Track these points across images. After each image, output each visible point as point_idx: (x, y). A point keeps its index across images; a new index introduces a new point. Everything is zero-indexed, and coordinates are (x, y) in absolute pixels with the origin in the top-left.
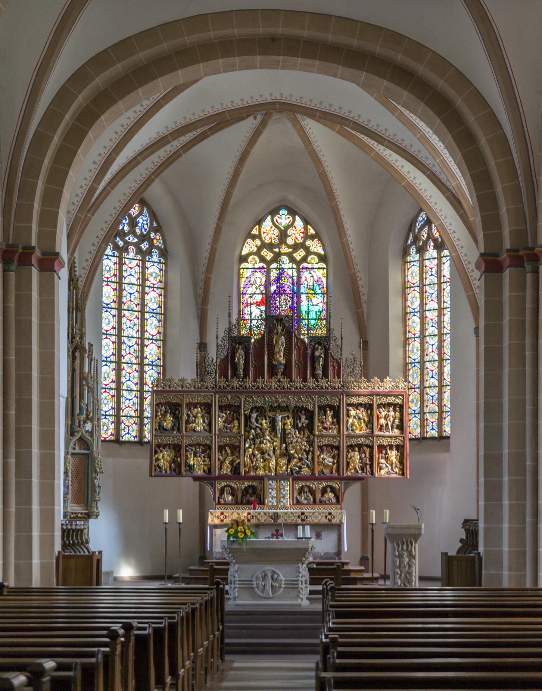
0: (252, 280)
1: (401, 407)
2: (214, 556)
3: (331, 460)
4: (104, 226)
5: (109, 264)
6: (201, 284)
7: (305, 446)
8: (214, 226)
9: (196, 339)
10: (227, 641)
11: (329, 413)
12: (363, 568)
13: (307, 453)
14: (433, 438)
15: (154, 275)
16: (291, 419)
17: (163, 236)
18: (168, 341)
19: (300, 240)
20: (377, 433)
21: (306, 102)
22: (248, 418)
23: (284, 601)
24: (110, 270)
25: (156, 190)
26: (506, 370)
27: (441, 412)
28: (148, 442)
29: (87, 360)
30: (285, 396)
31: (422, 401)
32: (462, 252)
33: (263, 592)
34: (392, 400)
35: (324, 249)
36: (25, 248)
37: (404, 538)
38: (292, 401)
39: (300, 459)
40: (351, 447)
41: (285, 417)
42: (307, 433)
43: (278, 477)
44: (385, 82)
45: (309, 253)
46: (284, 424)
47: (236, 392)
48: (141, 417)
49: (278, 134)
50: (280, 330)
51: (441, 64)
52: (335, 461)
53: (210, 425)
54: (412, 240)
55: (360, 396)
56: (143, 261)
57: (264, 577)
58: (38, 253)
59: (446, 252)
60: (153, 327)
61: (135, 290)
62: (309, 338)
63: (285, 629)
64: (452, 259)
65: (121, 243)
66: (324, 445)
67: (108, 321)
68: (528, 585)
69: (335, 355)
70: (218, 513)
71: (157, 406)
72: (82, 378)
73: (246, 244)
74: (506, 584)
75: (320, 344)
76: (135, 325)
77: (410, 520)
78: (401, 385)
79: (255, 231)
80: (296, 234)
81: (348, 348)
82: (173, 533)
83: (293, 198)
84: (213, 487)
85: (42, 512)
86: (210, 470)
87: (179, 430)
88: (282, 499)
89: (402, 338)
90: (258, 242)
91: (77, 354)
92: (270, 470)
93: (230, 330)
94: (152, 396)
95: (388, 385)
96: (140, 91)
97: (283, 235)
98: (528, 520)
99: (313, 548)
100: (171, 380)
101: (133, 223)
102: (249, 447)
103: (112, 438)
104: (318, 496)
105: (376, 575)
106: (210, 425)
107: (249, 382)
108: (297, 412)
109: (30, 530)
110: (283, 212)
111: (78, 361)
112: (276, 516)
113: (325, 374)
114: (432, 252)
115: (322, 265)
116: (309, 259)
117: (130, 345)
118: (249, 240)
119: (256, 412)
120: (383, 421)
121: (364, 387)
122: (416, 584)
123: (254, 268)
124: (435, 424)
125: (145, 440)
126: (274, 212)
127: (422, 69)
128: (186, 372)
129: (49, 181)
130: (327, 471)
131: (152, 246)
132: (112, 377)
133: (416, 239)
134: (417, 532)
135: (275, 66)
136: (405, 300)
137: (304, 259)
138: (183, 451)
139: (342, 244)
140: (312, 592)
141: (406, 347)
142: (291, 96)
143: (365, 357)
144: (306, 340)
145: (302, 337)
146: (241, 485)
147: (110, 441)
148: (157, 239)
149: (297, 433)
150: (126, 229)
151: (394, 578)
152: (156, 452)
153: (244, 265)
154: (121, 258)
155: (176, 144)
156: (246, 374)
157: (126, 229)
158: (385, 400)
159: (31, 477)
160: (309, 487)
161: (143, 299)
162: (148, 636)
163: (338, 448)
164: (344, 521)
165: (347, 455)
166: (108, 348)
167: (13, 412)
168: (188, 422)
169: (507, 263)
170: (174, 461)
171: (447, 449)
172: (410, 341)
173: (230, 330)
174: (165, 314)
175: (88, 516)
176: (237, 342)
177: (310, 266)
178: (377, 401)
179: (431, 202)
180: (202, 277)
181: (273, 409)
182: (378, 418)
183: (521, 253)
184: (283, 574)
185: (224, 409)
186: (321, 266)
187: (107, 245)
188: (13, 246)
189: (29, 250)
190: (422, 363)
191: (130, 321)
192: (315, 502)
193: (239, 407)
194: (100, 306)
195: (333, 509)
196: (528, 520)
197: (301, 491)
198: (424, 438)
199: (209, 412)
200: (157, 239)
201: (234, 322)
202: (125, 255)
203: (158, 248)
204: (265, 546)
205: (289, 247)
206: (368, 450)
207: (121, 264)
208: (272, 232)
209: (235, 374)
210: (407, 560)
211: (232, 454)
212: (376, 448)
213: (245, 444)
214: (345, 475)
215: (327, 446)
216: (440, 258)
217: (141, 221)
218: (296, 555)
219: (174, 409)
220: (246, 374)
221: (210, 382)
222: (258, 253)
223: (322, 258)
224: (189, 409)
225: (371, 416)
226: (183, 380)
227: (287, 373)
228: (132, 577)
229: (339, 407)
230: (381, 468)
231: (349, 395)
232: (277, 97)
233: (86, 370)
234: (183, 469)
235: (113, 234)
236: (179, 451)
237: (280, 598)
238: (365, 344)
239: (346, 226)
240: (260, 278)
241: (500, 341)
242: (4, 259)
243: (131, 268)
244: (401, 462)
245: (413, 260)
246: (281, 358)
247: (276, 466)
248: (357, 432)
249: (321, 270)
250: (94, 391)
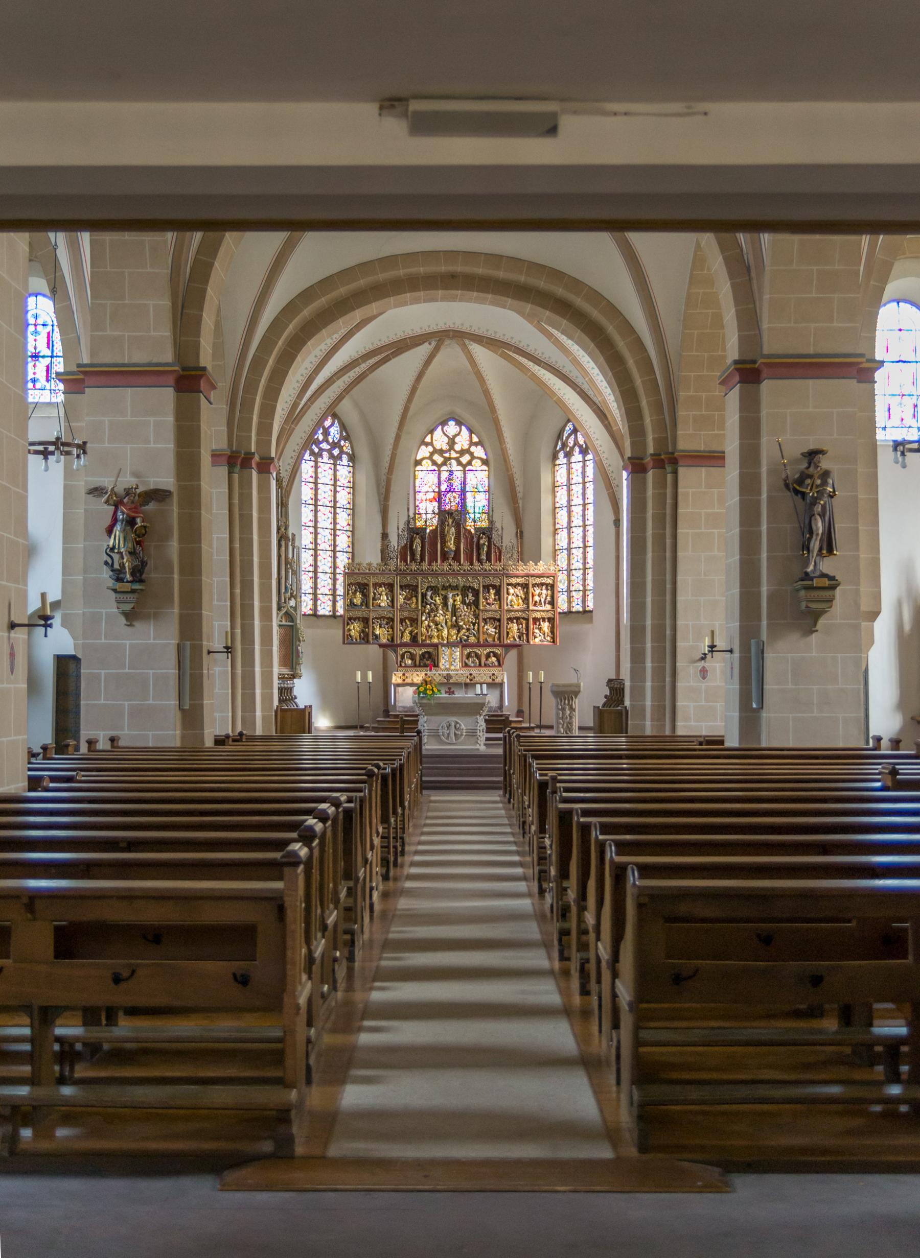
0: (426, 481)
1: (552, 586)
4: (303, 435)
5: (307, 468)
6: (384, 484)
7: (471, 618)
8: (394, 435)
9: (379, 530)
10: (424, 779)
12: (521, 719)
13: (474, 625)
14: (578, 612)
17: (351, 443)
18: (356, 532)
19: (466, 447)
20: (531, 607)
21: (475, 330)
22: (424, 596)
23: (464, 746)
25: (346, 407)
26: (649, 555)
27: (585, 591)
28: (341, 616)
29: (290, 548)
31: (569, 581)
32: (604, 456)
33: (447, 738)
34: (545, 580)
36: (246, 454)
37: (566, 695)
38: (461, 581)
39: (468, 630)
40: (510, 620)
42: (473, 608)
43: (450, 645)
44: (548, 313)
45: (473, 457)
46: (454, 601)
47: (414, 574)
48: (334, 595)
49: (450, 357)
51: (595, 297)
53: (392, 601)
54: (560, 446)
55: (517, 577)
56: (335, 465)
57: (449, 727)
58: (257, 458)
59: (590, 457)
60: (343, 519)
62: (475, 529)
63: (468, 769)
64: (595, 462)
65: (316, 450)
67: (307, 514)
68: (668, 733)
70: (400, 674)
71: (348, 586)
72: (287, 562)
74: (648, 732)
75: (484, 534)
77: (571, 679)
78: (552, 568)
79: (428, 439)
80: (463, 441)
81: (507, 537)
82: (364, 690)
83: (459, 411)
84: (396, 652)
85: (263, 673)
86: (393, 638)
87: (367, 606)
89: (552, 529)
90: (430, 449)
91: (283, 543)
92: (443, 639)
94: (344, 577)
95: (541, 568)
96: (341, 320)
97: (452, 442)
98: (668, 679)
99: (489, 702)
100: (359, 564)
101: (326, 433)
103: (311, 612)
104: (483, 659)
105: (532, 725)
106: (392, 601)
107: (425, 566)
108: (465, 590)
109: (254, 688)
110: (452, 423)
111: (283, 548)
113: (489, 559)
114: (577, 456)
115: (485, 468)
116: (474, 462)
117: (325, 536)
118: (423, 447)
120: (537, 598)
121: (522, 569)
122: (576, 733)
124: (580, 600)
125: (338, 614)
126: (444, 423)
127: (579, 302)
128: (371, 557)
129: (265, 396)
130: (490, 640)
131: (342, 452)
133: (564, 445)
134: (577, 689)
135: (453, 299)
136: (555, 497)
137: (469, 463)
138: (371, 623)
139: (502, 450)
140: (487, 739)
142: (462, 324)
143: (522, 543)
144: (473, 531)
145: (468, 528)
147: (309, 615)
148: (346, 445)
150: (321, 438)
151: (558, 727)
152: (348, 624)
153: (418, 468)
154: (316, 462)
155: (364, 366)
156: (422, 559)
157: (321, 438)
158: (538, 581)
159: (254, 644)
160: (494, 653)
162: (388, 773)
163: (499, 620)
164: (505, 680)
166: (306, 538)
167: (238, 591)
168: (374, 599)
169: (651, 465)
170: (363, 631)
171: (590, 620)
172: (559, 531)
173: (409, 522)
174: (353, 509)
175: (293, 676)
176: (414, 532)
178: (532, 581)
179: (578, 414)
180: (384, 478)
181: (444, 588)
182: (533, 596)
183: (663, 457)
184: (464, 724)
187: (306, 451)
188: (238, 452)
189: (249, 457)
190: (569, 549)
192: (480, 665)
193: (417, 586)
194: (300, 503)
195: (496, 671)
196: (668, 679)
197: (469, 656)
198: (570, 612)
199: (392, 591)
200: (346, 445)
201: (411, 515)
202: (320, 459)
203: (347, 454)
204: (461, 701)
205: (457, 452)
206: (524, 622)
207: (316, 467)
209: (413, 559)
210: (568, 712)
211: (411, 626)
212: (531, 621)
215: (490, 618)
216: (584, 461)
218: (474, 708)
219: (363, 588)
220: (422, 559)
221: (392, 565)
222: (430, 458)
223: (485, 462)
224: (375, 588)
225: (527, 594)
226: (370, 564)
227: (457, 558)
228: (329, 727)
229: (500, 586)
230: (535, 637)
231: (509, 576)
232: (450, 325)
233: (290, 556)
234: (371, 637)
235: (310, 441)
236: (367, 623)
237: (461, 744)
238: (520, 534)
239: (505, 435)
240: (433, 478)
241: (644, 530)
242: (229, 463)
244: (552, 632)
246: (451, 545)
248: (515, 607)
250: (296, 573)
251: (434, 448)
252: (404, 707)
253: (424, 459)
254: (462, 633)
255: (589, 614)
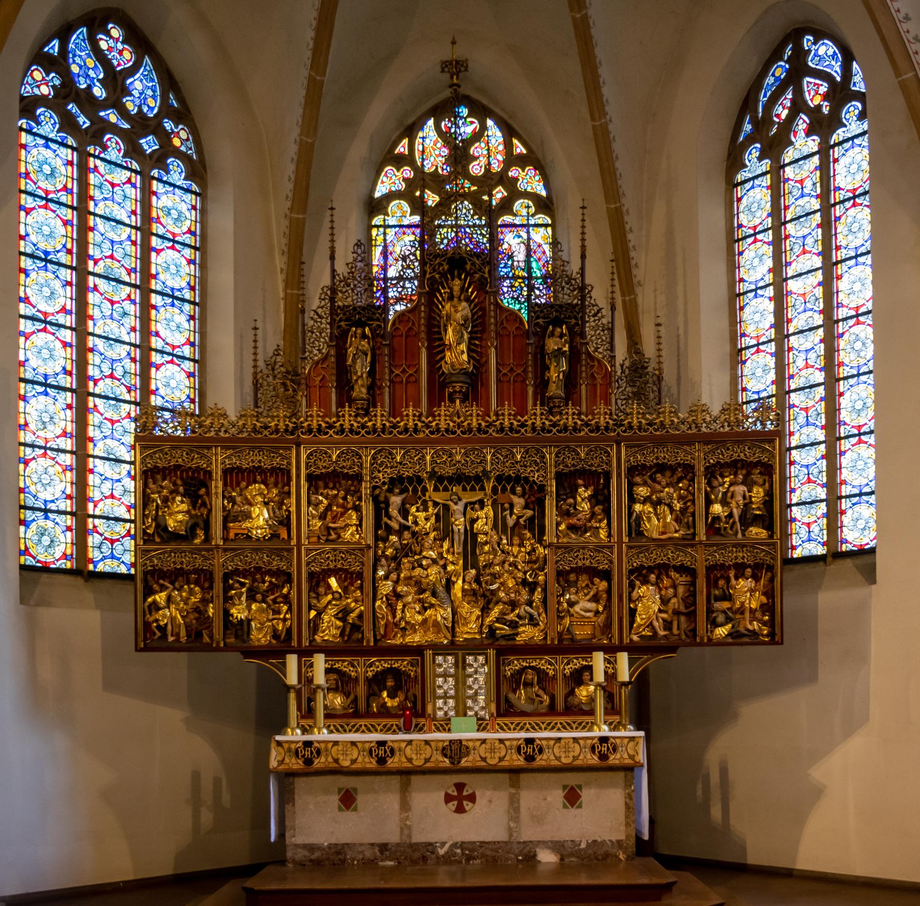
2: (289, 854)
3: (592, 606)
11: (584, 493)
15: (174, 214)
16: (489, 510)
17: (194, 132)
22: (381, 508)
24: (52, 174)
30: (474, 449)
35: (546, 186)
41: (474, 503)
43: (458, 649)
45: (514, 193)
50: (456, 289)
52: (601, 609)
61: (124, 236)
62: (531, 307)
65: (83, 121)
66: (573, 570)
69: (596, 349)
73: (382, 177)
76: (125, 314)
79: (402, 148)
88: (470, 703)
90: (408, 172)
93: (333, 290)
97: (459, 155)
102: (386, 577)
107: (380, 417)
112: (455, 750)
114: (804, 143)
116: (518, 205)
119: (401, 493)
123: (401, 226)
132: (63, 424)
133: (762, 125)
137: (506, 206)
141: (736, 370)
144: (524, 315)
146: (363, 669)
149: (505, 541)
153: (378, 220)
161: (145, 262)
165: (630, 593)
171: (870, 575)
177: (517, 221)
185: (321, 484)
186: (540, 222)
191: (112, 303)
200: (181, 138)
208: (437, 152)
213: (375, 571)
214: (626, 641)
215: (578, 571)
217: (138, 85)
219: (195, 485)
223: (544, 205)
243: (113, 185)
245: (751, 176)
246: (457, 355)
247: (453, 622)
249: (542, 230)
251: (419, 170)
252: (311, 848)
253: (390, 196)
254: (495, 612)
255: (866, 559)
